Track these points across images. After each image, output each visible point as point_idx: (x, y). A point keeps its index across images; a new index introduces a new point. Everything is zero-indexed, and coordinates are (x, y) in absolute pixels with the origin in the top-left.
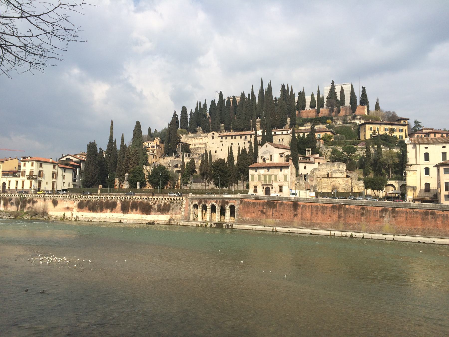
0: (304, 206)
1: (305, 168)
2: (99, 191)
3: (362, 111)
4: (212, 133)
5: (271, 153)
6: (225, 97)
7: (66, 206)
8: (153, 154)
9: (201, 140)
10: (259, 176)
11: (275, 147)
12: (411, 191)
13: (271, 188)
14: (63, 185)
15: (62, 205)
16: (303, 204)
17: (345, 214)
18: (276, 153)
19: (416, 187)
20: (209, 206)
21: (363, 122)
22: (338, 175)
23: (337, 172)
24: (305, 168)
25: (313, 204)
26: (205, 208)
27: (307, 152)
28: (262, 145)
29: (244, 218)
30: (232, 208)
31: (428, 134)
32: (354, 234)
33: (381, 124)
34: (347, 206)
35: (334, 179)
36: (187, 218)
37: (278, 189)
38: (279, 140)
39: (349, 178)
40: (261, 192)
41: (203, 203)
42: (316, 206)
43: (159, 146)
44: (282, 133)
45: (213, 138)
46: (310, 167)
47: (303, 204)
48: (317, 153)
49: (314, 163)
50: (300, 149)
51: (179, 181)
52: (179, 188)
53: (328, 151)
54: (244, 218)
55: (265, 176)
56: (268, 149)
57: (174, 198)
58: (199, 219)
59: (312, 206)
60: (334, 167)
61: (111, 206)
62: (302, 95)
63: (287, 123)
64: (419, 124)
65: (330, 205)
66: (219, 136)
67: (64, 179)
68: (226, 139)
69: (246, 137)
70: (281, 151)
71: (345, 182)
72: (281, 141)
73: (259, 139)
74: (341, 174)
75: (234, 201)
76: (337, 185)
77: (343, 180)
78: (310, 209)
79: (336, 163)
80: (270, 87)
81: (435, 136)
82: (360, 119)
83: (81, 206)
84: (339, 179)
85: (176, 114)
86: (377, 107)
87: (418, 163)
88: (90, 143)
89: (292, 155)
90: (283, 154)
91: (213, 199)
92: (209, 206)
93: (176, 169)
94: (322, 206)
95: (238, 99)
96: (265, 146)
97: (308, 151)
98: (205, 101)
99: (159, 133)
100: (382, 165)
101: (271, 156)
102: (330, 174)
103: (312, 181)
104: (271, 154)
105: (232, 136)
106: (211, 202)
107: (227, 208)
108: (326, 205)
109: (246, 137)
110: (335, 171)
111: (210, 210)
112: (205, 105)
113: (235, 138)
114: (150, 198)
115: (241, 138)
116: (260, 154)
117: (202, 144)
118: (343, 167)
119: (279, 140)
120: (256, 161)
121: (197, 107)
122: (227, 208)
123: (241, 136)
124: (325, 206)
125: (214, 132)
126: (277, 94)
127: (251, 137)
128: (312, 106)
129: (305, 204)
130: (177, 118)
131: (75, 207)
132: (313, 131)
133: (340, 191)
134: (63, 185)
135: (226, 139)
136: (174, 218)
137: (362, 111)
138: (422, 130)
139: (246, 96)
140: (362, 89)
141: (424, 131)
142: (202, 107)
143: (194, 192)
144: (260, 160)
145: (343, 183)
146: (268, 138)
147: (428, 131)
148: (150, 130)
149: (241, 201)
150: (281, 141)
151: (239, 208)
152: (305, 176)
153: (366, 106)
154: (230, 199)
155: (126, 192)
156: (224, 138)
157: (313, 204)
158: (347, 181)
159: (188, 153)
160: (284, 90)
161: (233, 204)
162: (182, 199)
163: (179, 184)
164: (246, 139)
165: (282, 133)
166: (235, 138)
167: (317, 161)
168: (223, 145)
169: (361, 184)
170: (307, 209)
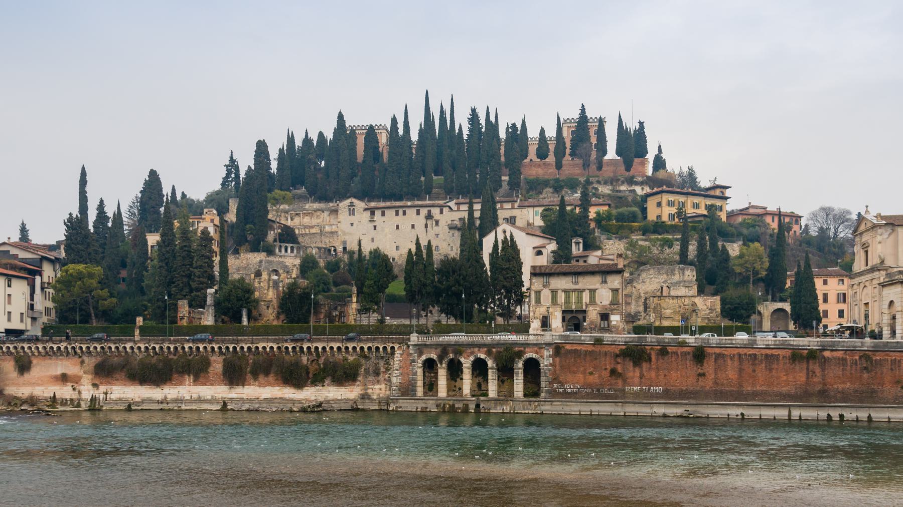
0: (719, 356)
2: (137, 332)
4: (349, 201)
7: (59, 371)
14: (9, 320)
15: (42, 369)
16: (718, 351)
17: (823, 370)
20: (467, 363)
21: (647, 190)
30: (532, 367)
33: (687, 194)
34: (827, 354)
36: (407, 390)
41: (452, 356)
42: (750, 355)
45: (352, 212)
58: (442, 392)
59: (740, 355)
61: (196, 369)
65: (788, 353)
66: (365, 210)
67: (9, 303)
68: (383, 214)
69: (429, 211)
71: (709, 304)
78: (736, 363)
83: (105, 371)
85: (664, 156)
91: (480, 346)
92: (467, 363)
94: (767, 355)
97: (578, 243)
102: (665, 288)
108: (774, 352)
109: (429, 211)
111: (470, 371)
113: (404, 213)
114: (305, 347)
115: (418, 213)
124: (772, 355)
125: (354, 200)
126: (462, 122)
127: (441, 212)
129: (723, 351)
131: (85, 373)
134: (9, 320)
135: (383, 214)
145: (705, 307)
151: (551, 365)
155: (215, 331)
156: (378, 213)
159: (289, 245)
160: (474, 118)
161: (534, 356)
162: (393, 348)
166: (404, 213)
168: (375, 227)
170: (729, 362)
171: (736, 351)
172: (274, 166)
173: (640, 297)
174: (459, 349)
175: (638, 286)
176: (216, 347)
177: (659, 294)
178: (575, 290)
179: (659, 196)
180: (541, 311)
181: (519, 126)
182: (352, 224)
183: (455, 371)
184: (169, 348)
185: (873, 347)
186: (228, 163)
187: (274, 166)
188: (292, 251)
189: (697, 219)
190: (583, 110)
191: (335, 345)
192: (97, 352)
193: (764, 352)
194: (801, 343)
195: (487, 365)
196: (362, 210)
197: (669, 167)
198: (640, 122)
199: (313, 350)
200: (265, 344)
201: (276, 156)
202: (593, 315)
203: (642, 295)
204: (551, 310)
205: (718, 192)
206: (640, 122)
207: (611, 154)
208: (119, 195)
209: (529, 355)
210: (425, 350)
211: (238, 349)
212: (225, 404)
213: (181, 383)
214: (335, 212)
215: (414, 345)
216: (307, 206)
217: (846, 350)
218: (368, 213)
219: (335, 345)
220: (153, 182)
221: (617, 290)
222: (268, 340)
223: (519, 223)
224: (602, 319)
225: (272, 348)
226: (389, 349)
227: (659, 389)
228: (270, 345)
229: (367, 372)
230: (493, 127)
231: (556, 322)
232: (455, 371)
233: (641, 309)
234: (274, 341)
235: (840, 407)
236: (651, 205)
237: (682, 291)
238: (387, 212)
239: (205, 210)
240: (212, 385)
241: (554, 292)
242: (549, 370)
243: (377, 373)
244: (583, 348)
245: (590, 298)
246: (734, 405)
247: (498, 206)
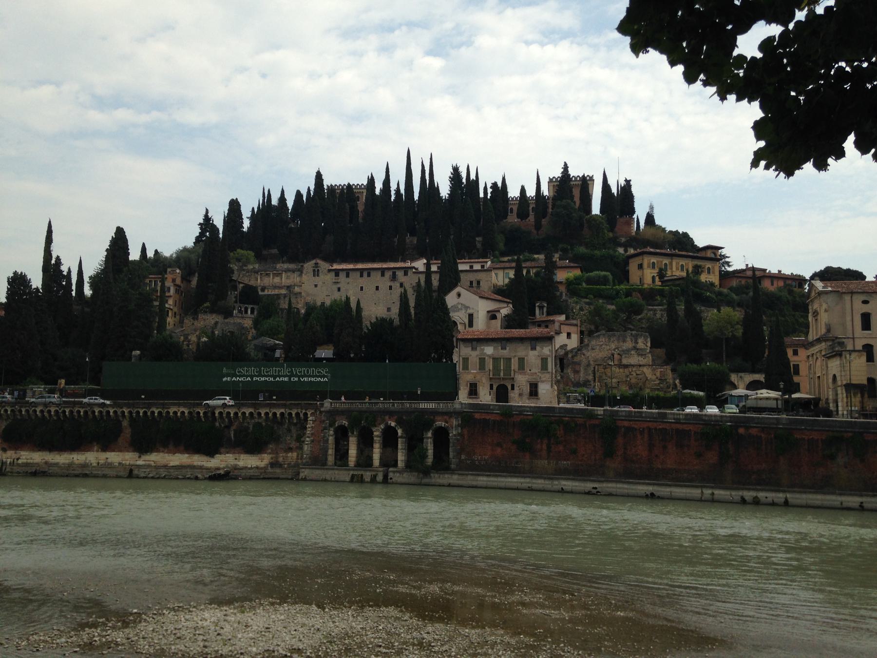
0: (629, 429)
4: (314, 261)
6: (327, 182)
9: (277, 280)
10: (482, 361)
11: (480, 297)
13: (509, 387)
16: (626, 424)
23: (633, 352)
25: (650, 424)
29: (475, 458)
30: (441, 436)
32: (716, 492)
37: (527, 389)
38: (471, 283)
40: (486, 397)
43: (180, 286)
44: (471, 267)
48: (561, 313)
54: (475, 458)
55: (496, 360)
56: (462, 300)
57: (282, 410)
59: (650, 429)
60: (624, 341)
64: (727, 260)
68: (348, 276)
71: (658, 374)
72: (475, 284)
74: (640, 359)
75: (446, 417)
77: (654, 370)
78: (646, 436)
85: (210, 215)
86: (650, 219)
88: (15, 273)
91: (391, 414)
97: (541, 308)
98: (283, 192)
104: (470, 311)
105: (361, 271)
106: (384, 420)
108: (685, 427)
109: (394, 273)
110: (627, 352)
113: (369, 275)
117: (280, 288)
119: (471, 283)
123: (383, 271)
125: (319, 261)
132: (551, 267)
135: (348, 276)
136: (281, 459)
145: (654, 377)
148: (144, 249)
150: (475, 284)
151: (459, 434)
154: (434, 413)
156: (342, 275)
157: (652, 425)
159: (250, 307)
162: (306, 414)
164: (394, 278)
165: (471, 267)
171: (645, 425)
172: (246, 224)
173: (589, 365)
174: (374, 417)
175: (588, 354)
176: (126, 411)
179: (640, 258)
181: (500, 185)
182: (316, 286)
183: (366, 442)
184: (79, 412)
186: (202, 221)
187: (246, 224)
188: (252, 312)
189: (677, 282)
190: (566, 167)
191: (248, 411)
192: (8, 415)
193: (674, 426)
196: (326, 271)
198: (626, 180)
199: (224, 415)
200: (282, 410)
201: (249, 215)
203: (592, 363)
204: (478, 377)
205: (709, 254)
206: (626, 180)
208: (723, 252)
211: (149, 414)
212: (131, 471)
213: (88, 450)
214: (301, 271)
215: (326, 412)
216: (278, 266)
218: (333, 274)
219: (248, 411)
220: (119, 241)
222: (179, 405)
223: (484, 286)
225: (183, 413)
226: (302, 415)
228: (182, 409)
230: (474, 184)
232: (366, 442)
233: (591, 377)
234: (185, 406)
236: (633, 267)
237: (634, 359)
238: (372, 273)
239: (169, 270)
240: (120, 451)
242: (458, 440)
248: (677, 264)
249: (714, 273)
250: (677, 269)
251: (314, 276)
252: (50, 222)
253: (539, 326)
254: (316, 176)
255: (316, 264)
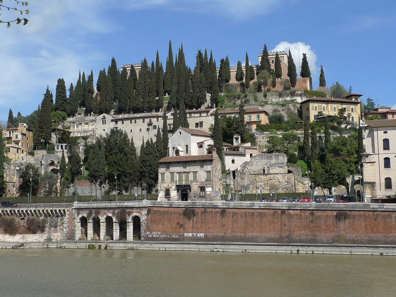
0: (235, 214)
1: (233, 161)
3: (303, 85)
5: (189, 143)
8: (17, 146)
11: (193, 135)
12: (369, 187)
18: (194, 141)
19: (375, 183)
20: (102, 219)
21: (305, 99)
22: (277, 170)
24: (233, 161)
26: (97, 224)
27: (234, 140)
28: (173, 131)
30: (136, 220)
31: (384, 115)
35: (272, 176)
39: (291, 174)
42: (251, 213)
46: (240, 161)
47: (234, 210)
49: (244, 155)
50: (227, 135)
51: (58, 184)
52: (58, 195)
53: (262, 139)
57: (51, 209)
59: (245, 213)
60: (272, 159)
62: (225, 64)
63: (206, 101)
69: (150, 120)
70: (201, 139)
71: (286, 179)
73: (170, 121)
74: (281, 169)
76: (276, 183)
77: (284, 176)
79: (274, 154)
80: (181, 53)
81: (393, 117)
82: (301, 95)
84: (278, 176)
87: (376, 152)
89: (215, 145)
90: (203, 142)
92: (102, 219)
93: (51, 168)
94: (260, 213)
95: (138, 69)
96: (177, 132)
97: (237, 139)
99: (23, 117)
100: (329, 156)
101: (187, 146)
102: (266, 169)
103: (243, 179)
105: (131, 119)
107: (130, 219)
109: (150, 120)
112: (91, 77)
113: (135, 122)
115: (144, 122)
116: (170, 146)
118: (283, 159)
120: (166, 154)
121: (79, 81)
122: (130, 219)
123: (143, 118)
125: (105, 115)
126: (191, 63)
127: (158, 120)
128: (239, 78)
130: (51, 96)
133: (280, 191)
137: (303, 85)
138: (377, 109)
139: (149, 65)
140: (302, 56)
141: (380, 110)
142: (87, 79)
143: (81, 199)
144: (172, 153)
146: (181, 123)
147: (385, 110)
149: (149, 210)
152: (234, 172)
153: (308, 78)
158: (289, 178)
161: (137, 214)
162: (64, 211)
163: (59, 189)
166: (135, 122)
167: (248, 152)
169: (307, 182)
172: (68, 94)
177: (262, 172)
178: (185, 172)
180: (165, 185)
185: (316, 207)
187: (68, 94)
194: (278, 205)
195: (112, 220)
196: (110, 121)
197: (22, 115)
202: (195, 188)
207: (233, 80)
209: (134, 214)
210: (81, 212)
217: (301, 210)
221: (209, 172)
224: (201, 190)
227: (202, 235)
229: (51, 226)
231: (174, 194)
235: (360, 246)
241: (172, 173)
243: (56, 227)
244: (162, 209)
245: (194, 177)
246: (365, 246)
247: (188, 115)
248: (331, 107)
249: (355, 111)
250: (331, 110)
251: (103, 124)
252: (206, 49)
253: (234, 150)
254: (112, 61)
255: (104, 117)
